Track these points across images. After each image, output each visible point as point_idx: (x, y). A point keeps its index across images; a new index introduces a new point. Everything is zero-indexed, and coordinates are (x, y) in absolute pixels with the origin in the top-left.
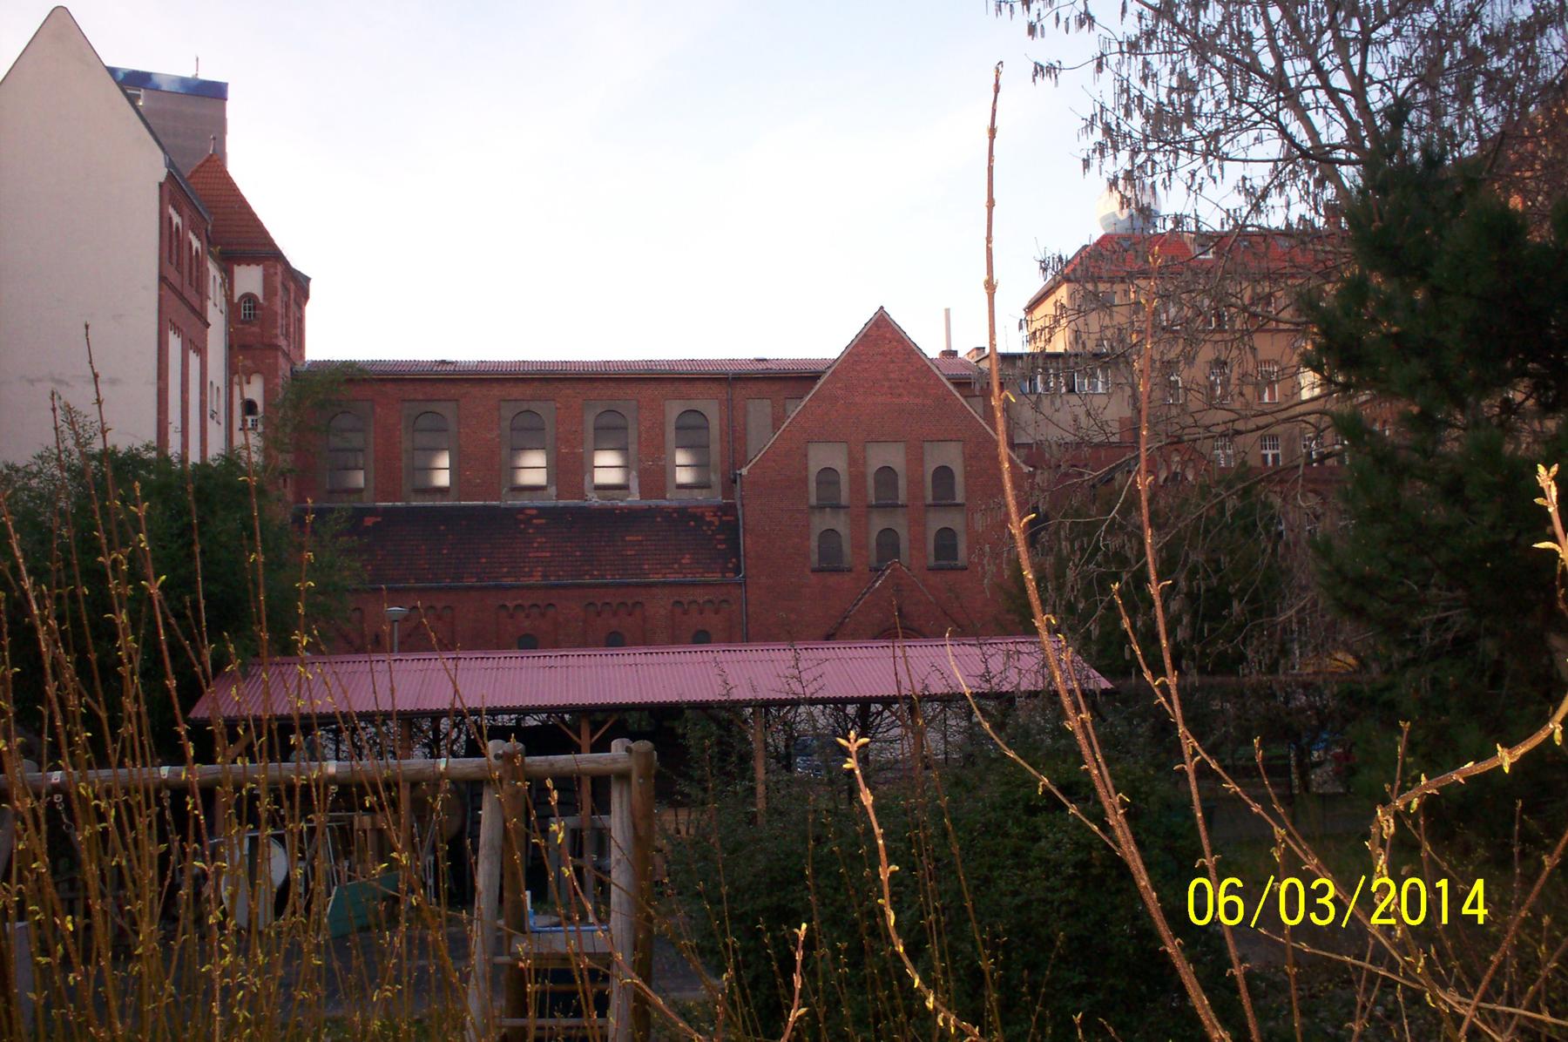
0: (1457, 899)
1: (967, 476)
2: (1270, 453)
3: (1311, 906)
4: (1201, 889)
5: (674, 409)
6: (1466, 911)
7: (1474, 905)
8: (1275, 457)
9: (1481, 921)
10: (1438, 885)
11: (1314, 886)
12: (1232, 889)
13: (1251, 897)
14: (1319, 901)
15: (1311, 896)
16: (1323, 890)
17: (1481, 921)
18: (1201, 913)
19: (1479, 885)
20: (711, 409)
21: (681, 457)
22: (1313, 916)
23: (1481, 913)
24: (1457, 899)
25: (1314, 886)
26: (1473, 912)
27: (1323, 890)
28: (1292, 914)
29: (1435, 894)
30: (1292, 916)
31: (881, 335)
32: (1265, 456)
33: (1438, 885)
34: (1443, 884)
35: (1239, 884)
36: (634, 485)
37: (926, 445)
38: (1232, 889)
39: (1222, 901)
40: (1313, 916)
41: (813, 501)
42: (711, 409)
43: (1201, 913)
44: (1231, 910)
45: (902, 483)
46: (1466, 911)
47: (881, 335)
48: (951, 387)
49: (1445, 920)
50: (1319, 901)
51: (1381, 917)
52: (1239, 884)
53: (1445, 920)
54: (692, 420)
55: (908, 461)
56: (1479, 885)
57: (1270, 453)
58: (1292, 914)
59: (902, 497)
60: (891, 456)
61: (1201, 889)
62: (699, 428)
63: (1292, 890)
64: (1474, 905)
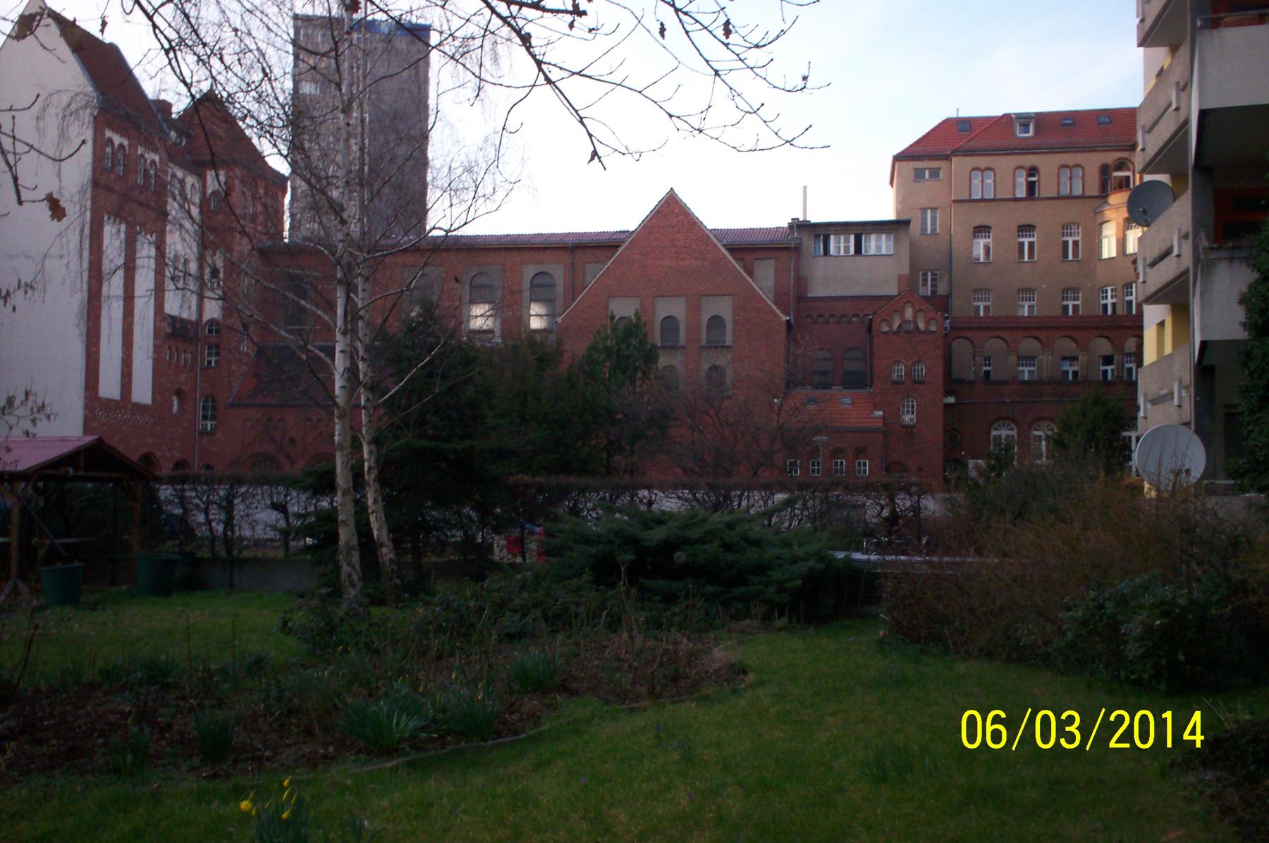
0: (1179, 728)
1: (735, 322)
2: (1070, 304)
3: (1061, 732)
4: (972, 720)
5: (529, 271)
6: (1186, 737)
7: (1193, 732)
8: (1076, 308)
9: (1198, 745)
10: (1164, 716)
11: (1064, 717)
12: (996, 720)
13: (1011, 724)
14: (1068, 729)
15: (1061, 725)
16: (1071, 720)
17: (1198, 745)
18: (972, 739)
19: (1197, 716)
20: (558, 272)
21: (535, 309)
22: (1063, 741)
23: (1199, 738)
24: (1179, 728)
25: (1064, 717)
26: (1192, 738)
27: (1071, 720)
28: (1046, 739)
29: (1161, 724)
30: (1046, 741)
31: (671, 211)
32: (1066, 307)
33: (1164, 716)
34: (1168, 715)
35: (1003, 715)
36: (498, 333)
37: (704, 300)
38: (996, 720)
39: (989, 729)
40: (1063, 741)
41: (704, 342)
42: (558, 272)
43: (972, 739)
44: (996, 736)
45: (682, 328)
46: (1186, 737)
47: (671, 211)
48: (726, 252)
49: (1169, 745)
50: (1068, 729)
51: (1117, 742)
52: (1003, 715)
53: (1169, 745)
54: (540, 280)
55: (688, 312)
56: (1197, 716)
57: (1070, 304)
58: (1046, 739)
59: (682, 340)
60: (674, 307)
61: (972, 720)
62: (549, 286)
63: (1046, 719)
64: (1193, 732)
